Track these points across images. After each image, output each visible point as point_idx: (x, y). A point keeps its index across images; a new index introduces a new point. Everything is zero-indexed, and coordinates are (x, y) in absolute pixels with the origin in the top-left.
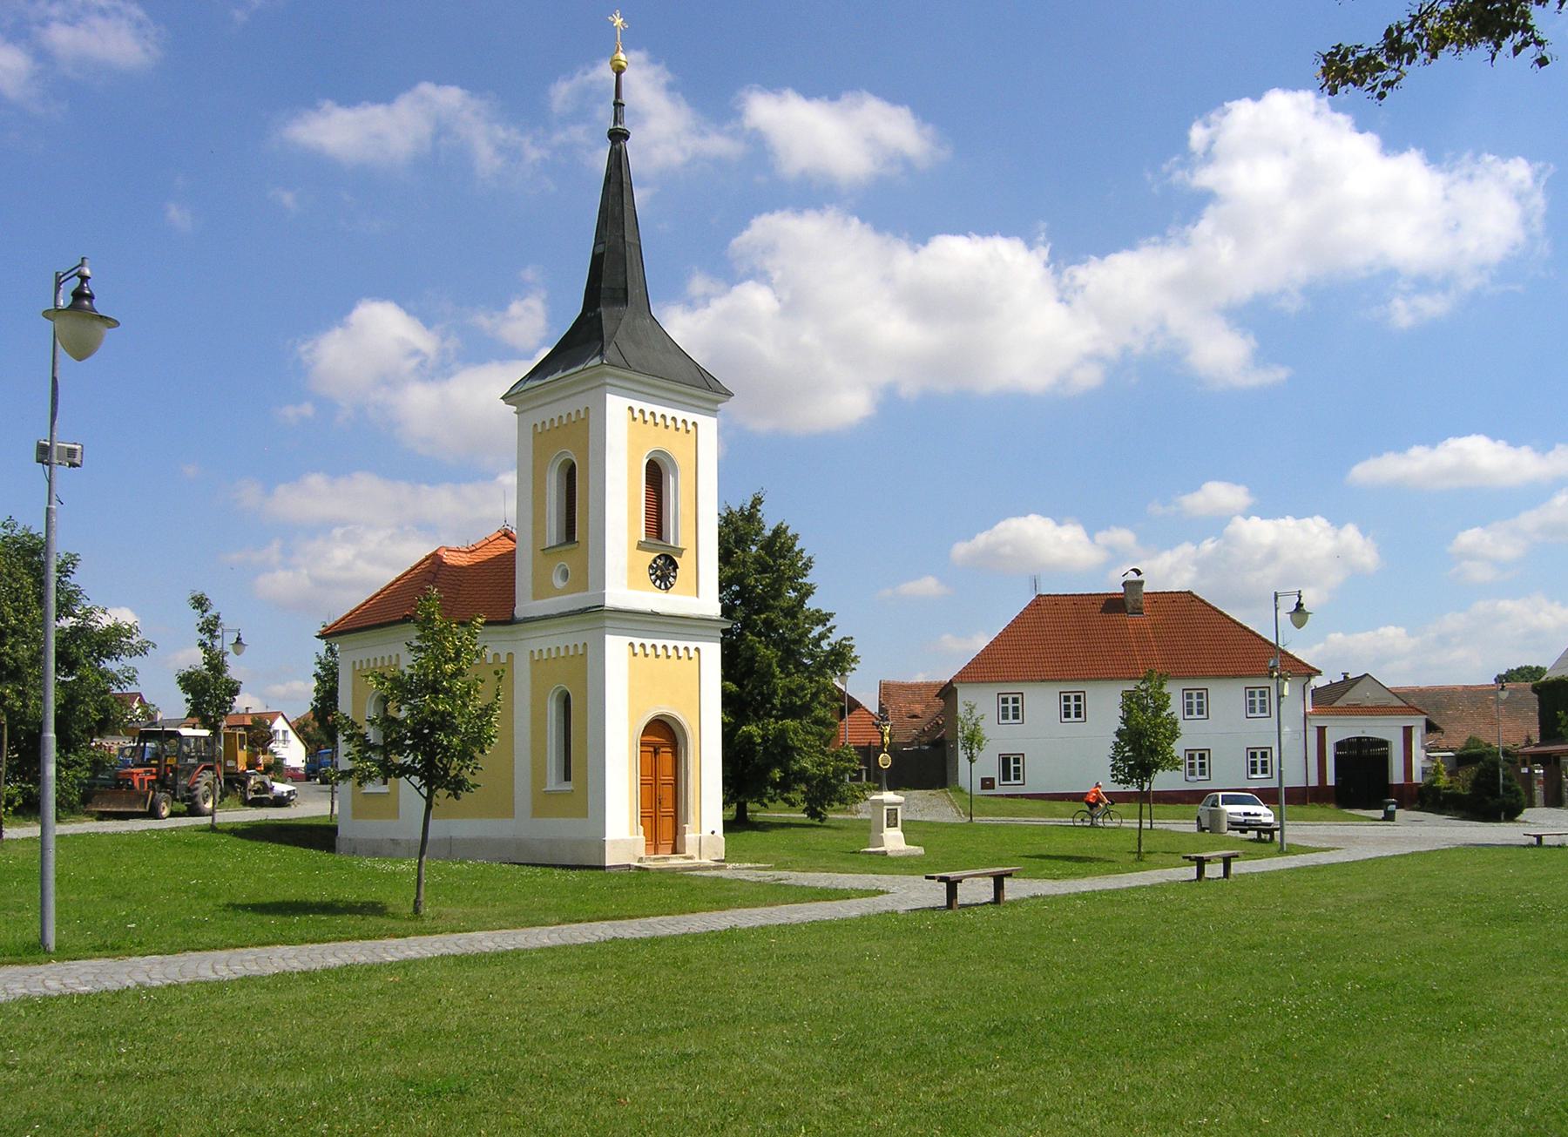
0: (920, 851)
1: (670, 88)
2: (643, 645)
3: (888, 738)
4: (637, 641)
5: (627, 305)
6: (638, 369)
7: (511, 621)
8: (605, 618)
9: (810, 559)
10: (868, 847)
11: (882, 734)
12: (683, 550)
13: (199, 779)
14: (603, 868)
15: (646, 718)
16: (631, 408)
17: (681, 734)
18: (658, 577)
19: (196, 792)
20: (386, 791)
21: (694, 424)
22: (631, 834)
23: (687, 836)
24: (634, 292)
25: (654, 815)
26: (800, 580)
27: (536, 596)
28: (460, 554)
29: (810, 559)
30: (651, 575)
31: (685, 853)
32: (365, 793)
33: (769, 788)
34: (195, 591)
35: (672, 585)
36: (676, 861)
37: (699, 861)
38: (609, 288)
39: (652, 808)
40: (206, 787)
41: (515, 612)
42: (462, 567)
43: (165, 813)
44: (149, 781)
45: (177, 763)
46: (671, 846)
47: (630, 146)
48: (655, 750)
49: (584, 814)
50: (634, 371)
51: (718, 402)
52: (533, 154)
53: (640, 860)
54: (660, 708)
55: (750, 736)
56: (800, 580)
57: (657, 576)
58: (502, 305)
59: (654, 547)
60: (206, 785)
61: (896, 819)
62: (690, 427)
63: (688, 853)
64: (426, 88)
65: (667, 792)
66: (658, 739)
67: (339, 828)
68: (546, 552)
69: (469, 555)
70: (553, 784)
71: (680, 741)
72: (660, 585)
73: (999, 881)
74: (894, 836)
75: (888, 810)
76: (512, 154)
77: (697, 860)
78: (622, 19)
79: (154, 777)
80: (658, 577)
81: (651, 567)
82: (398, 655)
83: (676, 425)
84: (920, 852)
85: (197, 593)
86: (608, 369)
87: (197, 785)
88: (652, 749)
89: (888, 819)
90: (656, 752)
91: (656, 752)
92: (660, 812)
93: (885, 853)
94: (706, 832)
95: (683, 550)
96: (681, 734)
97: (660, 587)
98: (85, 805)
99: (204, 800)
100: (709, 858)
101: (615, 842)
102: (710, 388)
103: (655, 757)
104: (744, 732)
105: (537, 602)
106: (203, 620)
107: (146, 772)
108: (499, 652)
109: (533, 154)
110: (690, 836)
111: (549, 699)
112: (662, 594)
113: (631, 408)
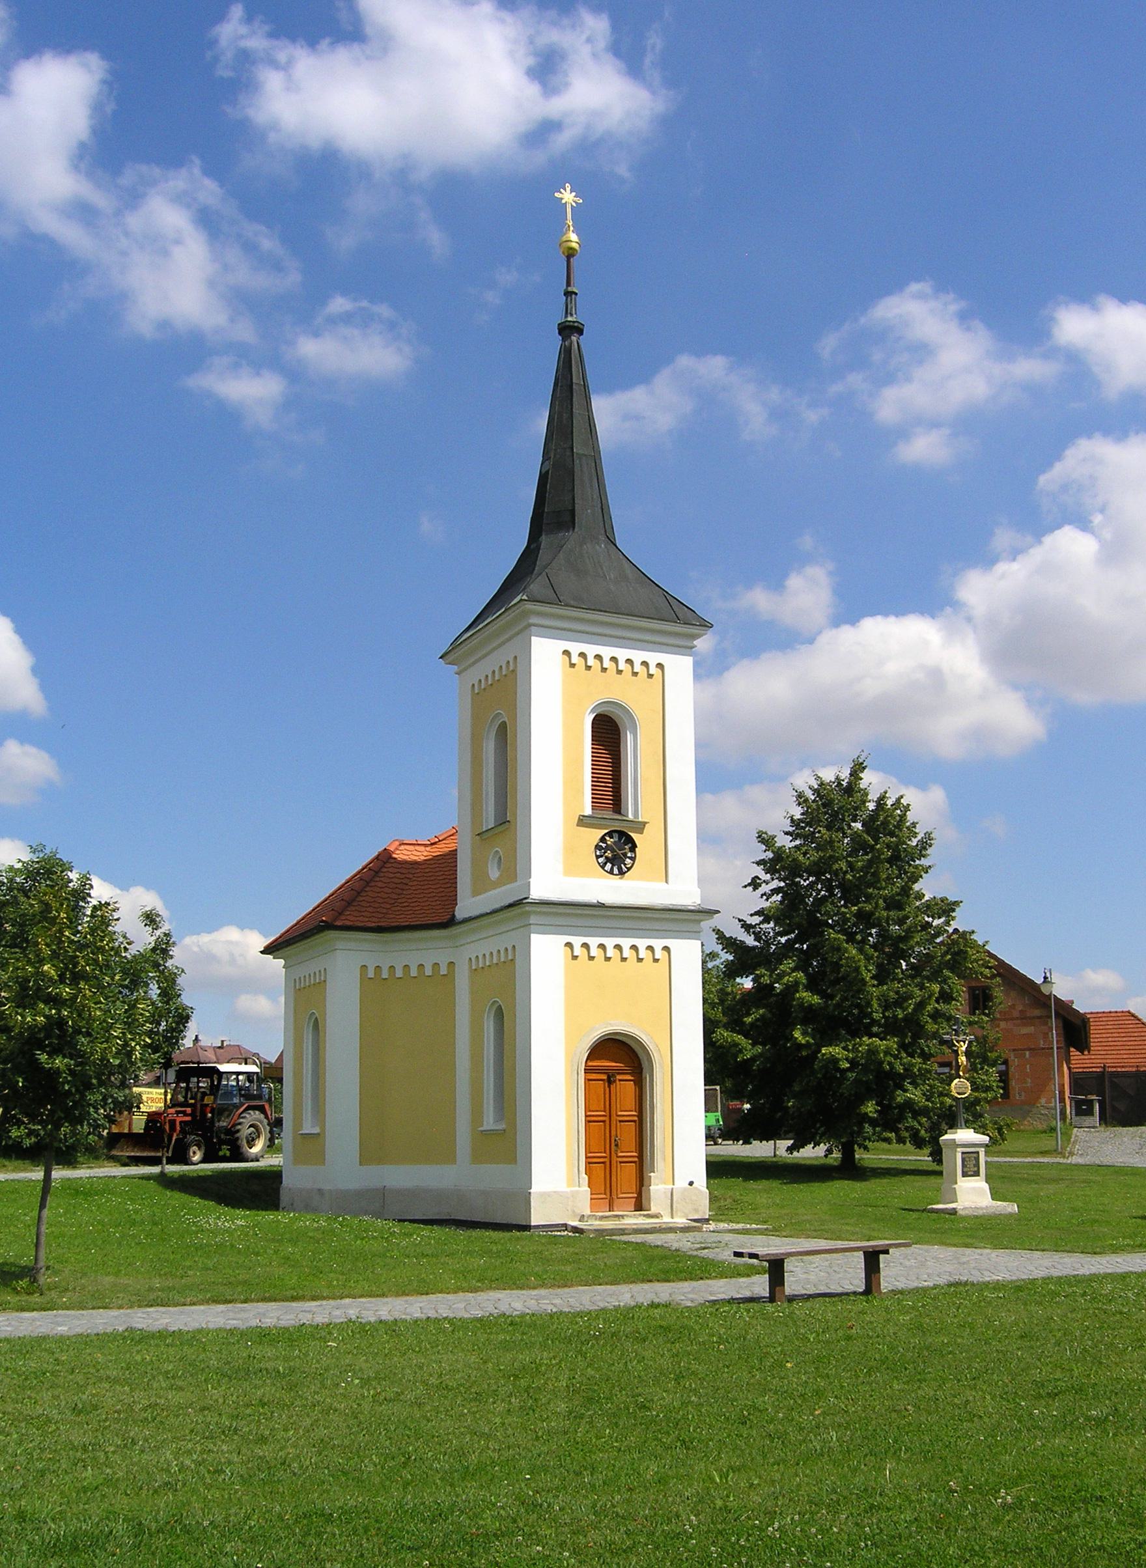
0: (1013, 1208)
1: (964, 318)
2: (586, 946)
3: (964, 1059)
4: (577, 941)
5: (574, 528)
6: (572, 603)
7: (450, 922)
8: (529, 913)
9: (928, 835)
10: (938, 1203)
11: (956, 1052)
12: (644, 824)
13: (241, 1120)
14: (527, 1228)
15: (592, 1037)
16: (567, 653)
17: (645, 1058)
18: (608, 860)
19: (238, 1135)
20: (316, 1132)
21: (660, 666)
22: (569, 1185)
23: (651, 1188)
24: (585, 513)
25: (607, 1160)
26: (918, 862)
27: (476, 893)
28: (417, 848)
29: (928, 835)
30: (598, 857)
31: (650, 1210)
32: (302, 1134)
33: (867, 1125)
34: (144, 906)
35: (629, 869)
36: (634, 1220)
37: (670, 1220)
38: (554, 512)
39: (605, 1152)
40: (252, 1129)
41: (456, 913)
42: (415, 863)
43: (196, 1158)
44: (181, 1122)
45: (214, 1102)
46: (634, 1200)
47: (587, 342)
48: (609, 1077)
49: (513, 1160)
50: (566, 605)
51: (695, 637)
52: (812, 417)
53: (582, 1218)
54: (611, 1025)
55: (834, 1061)
56: (918, 862)
57: (606, 857)
58: (777, 584)
59: (603, 822)
60: (251, 1126)
61: (977, 1165)
62: (653, 670)
63: (654, 1209)
64: (684, 361)
65: (627, 1134)
66: (614, 1064)
67: (283, 1173)
68: (485, 836)
69: (428, 849)
70: (491, 1120)
71: (645, 1064)
72: (612, 869)
73: (872, 1260)
74: (974, 1189)
75: (963, 1153)
76: (777, 414)
77: (666, 1219)
78: (574, 194)
79: (188, 1119)
80: (608, 860)
81: (597, 847)
82: (325, 969)
83: (648, 671)
84: (1010, 1210)
85: (148, 909)
86: (530, 606)
87: (239, 1127)
88: (605, 1077)
89: (964, 1166)
90: (610, 1081)
91: (610, 1081)
92: (617, 1157)
93: (954, 1212)
94: (681, 1183)
95: (644, 824)
96: (645, 1058)
97: (611, 872)
98: (110, 1150)
99: (248, 1142)
100: (685, 1216)
101: (544, 1195)
102: (677, 619)
103: (609, 1087)
104: (824, 1055)
105: (478, 898)
106: (154, 938)
107: (178, 1112)
108: (439, 962)
109: (812, 417)
110: (657, 1188)
111: (485, 1018)
112: (615, 881)
113: (567, 653)
